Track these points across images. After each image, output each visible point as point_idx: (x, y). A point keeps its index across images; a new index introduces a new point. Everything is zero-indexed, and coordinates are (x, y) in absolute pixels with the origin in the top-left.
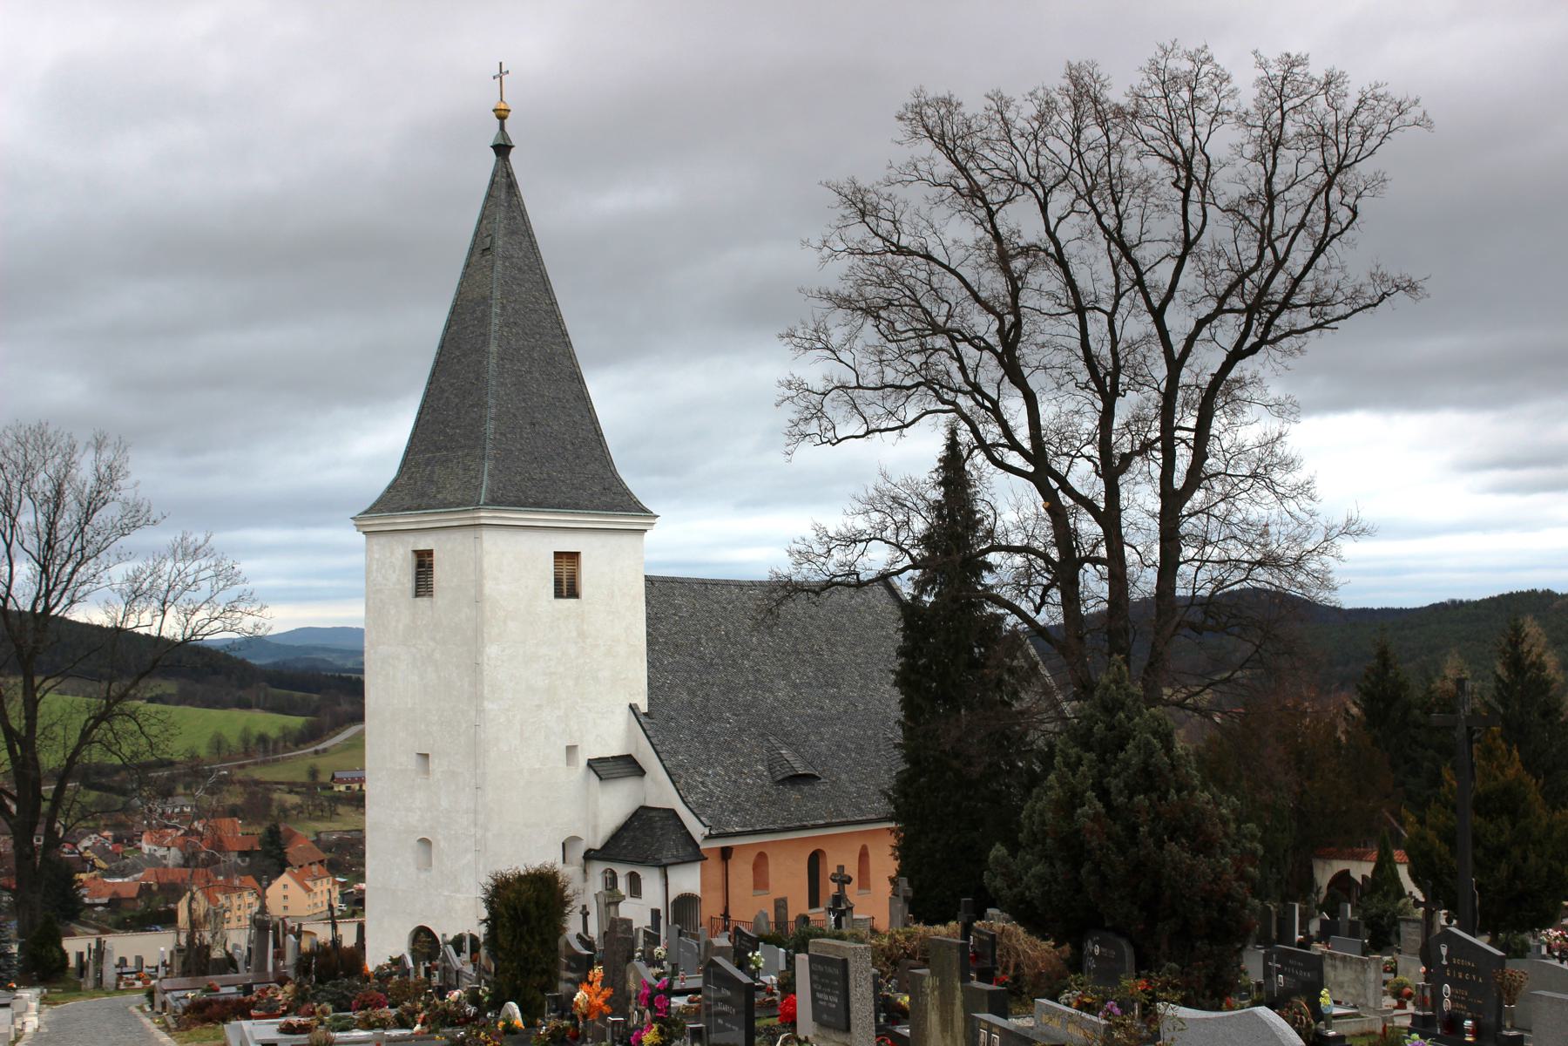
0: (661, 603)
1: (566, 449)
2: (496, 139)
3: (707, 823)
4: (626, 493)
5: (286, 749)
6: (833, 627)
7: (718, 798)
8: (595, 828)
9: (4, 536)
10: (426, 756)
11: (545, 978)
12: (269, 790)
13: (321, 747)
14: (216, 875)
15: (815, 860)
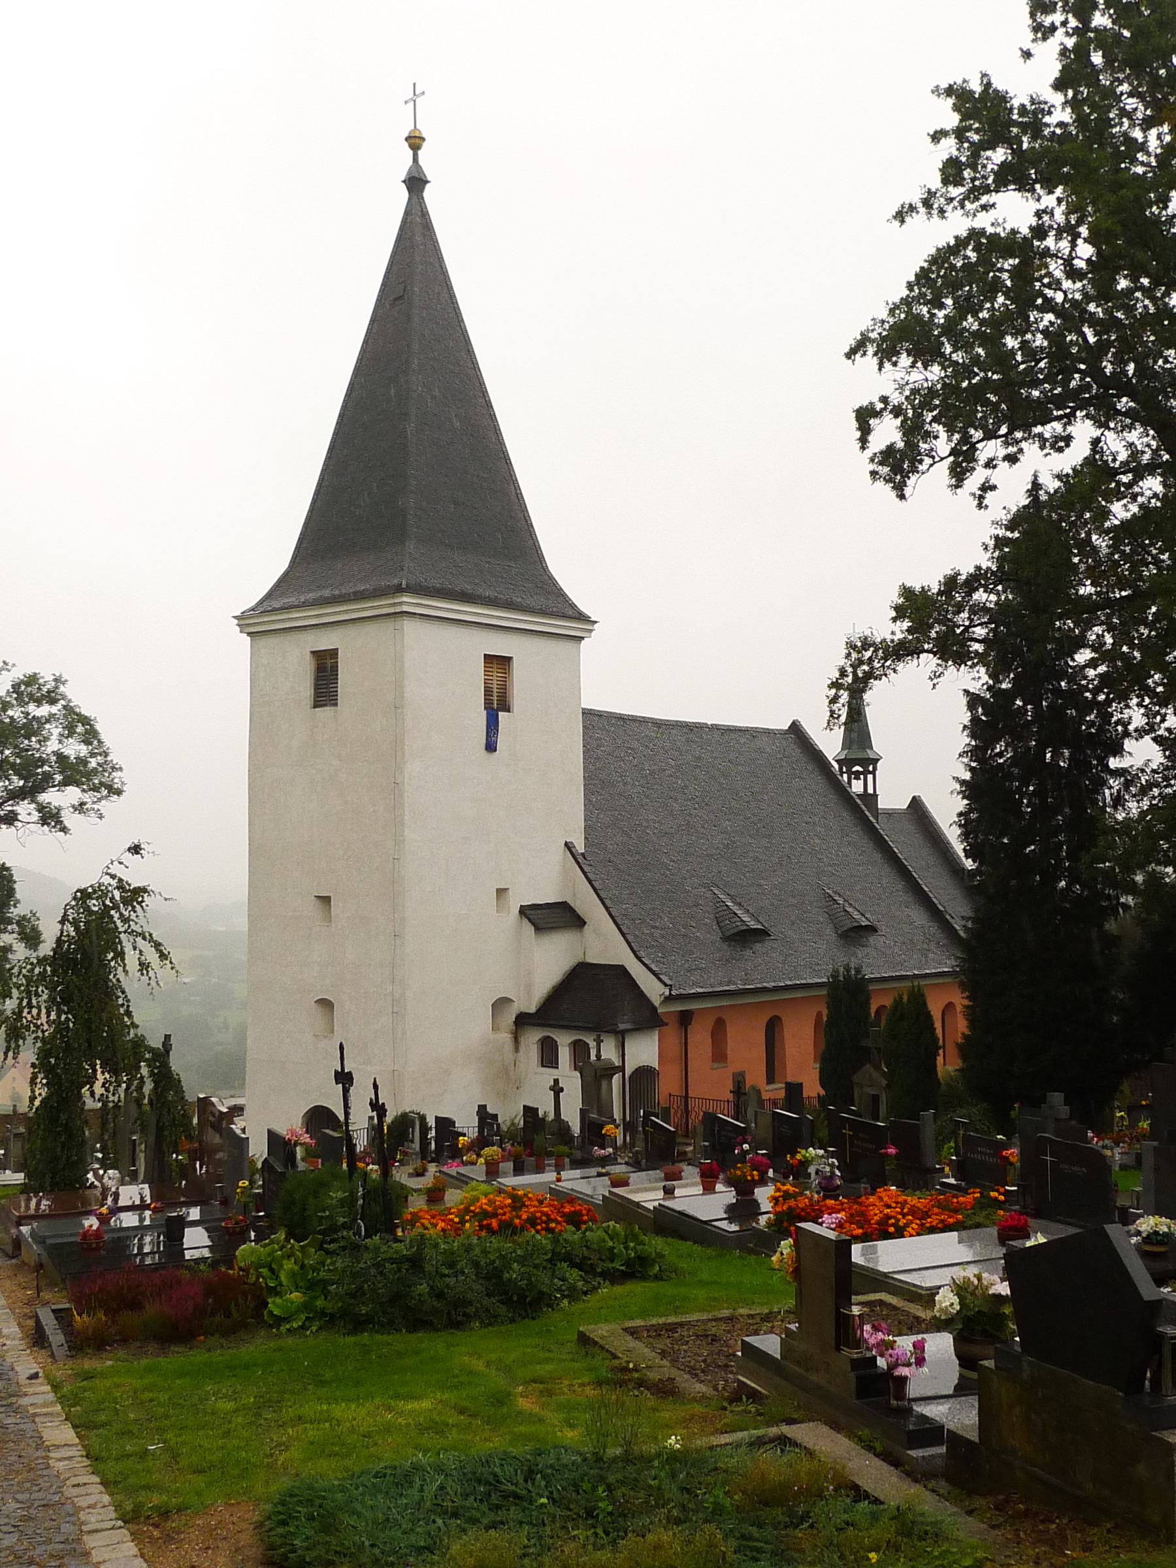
8: (529, 987)
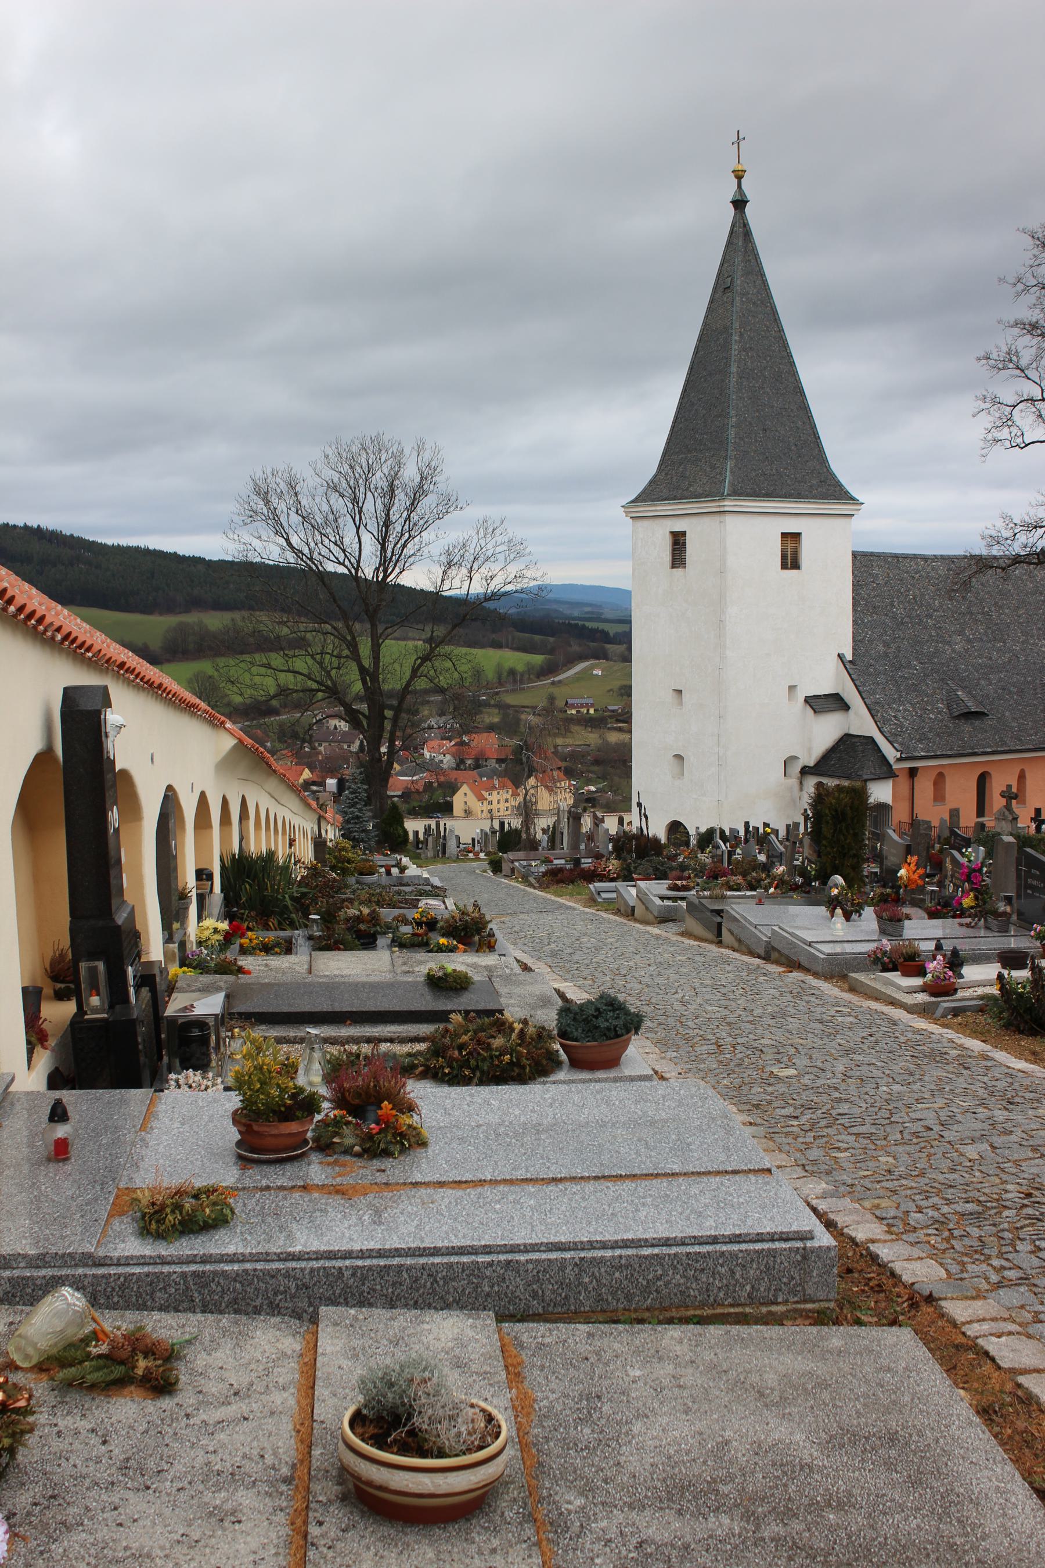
0: (862, 573)
1: (790, 449)
2: (735, 195)
3: (899, 748)
4: (839, 485)
5: (530, 681)
6: (1000, 593)
7: (907, 729)
8: (810, 750)
9: (354, 520)
10: (680, 692)
11: (855, 860)
12: (517, 711)
13: (557, 679)
14: (481, 776)
15: (983, 781)
